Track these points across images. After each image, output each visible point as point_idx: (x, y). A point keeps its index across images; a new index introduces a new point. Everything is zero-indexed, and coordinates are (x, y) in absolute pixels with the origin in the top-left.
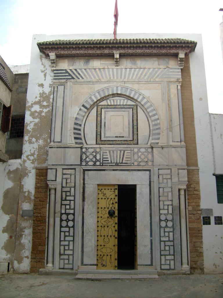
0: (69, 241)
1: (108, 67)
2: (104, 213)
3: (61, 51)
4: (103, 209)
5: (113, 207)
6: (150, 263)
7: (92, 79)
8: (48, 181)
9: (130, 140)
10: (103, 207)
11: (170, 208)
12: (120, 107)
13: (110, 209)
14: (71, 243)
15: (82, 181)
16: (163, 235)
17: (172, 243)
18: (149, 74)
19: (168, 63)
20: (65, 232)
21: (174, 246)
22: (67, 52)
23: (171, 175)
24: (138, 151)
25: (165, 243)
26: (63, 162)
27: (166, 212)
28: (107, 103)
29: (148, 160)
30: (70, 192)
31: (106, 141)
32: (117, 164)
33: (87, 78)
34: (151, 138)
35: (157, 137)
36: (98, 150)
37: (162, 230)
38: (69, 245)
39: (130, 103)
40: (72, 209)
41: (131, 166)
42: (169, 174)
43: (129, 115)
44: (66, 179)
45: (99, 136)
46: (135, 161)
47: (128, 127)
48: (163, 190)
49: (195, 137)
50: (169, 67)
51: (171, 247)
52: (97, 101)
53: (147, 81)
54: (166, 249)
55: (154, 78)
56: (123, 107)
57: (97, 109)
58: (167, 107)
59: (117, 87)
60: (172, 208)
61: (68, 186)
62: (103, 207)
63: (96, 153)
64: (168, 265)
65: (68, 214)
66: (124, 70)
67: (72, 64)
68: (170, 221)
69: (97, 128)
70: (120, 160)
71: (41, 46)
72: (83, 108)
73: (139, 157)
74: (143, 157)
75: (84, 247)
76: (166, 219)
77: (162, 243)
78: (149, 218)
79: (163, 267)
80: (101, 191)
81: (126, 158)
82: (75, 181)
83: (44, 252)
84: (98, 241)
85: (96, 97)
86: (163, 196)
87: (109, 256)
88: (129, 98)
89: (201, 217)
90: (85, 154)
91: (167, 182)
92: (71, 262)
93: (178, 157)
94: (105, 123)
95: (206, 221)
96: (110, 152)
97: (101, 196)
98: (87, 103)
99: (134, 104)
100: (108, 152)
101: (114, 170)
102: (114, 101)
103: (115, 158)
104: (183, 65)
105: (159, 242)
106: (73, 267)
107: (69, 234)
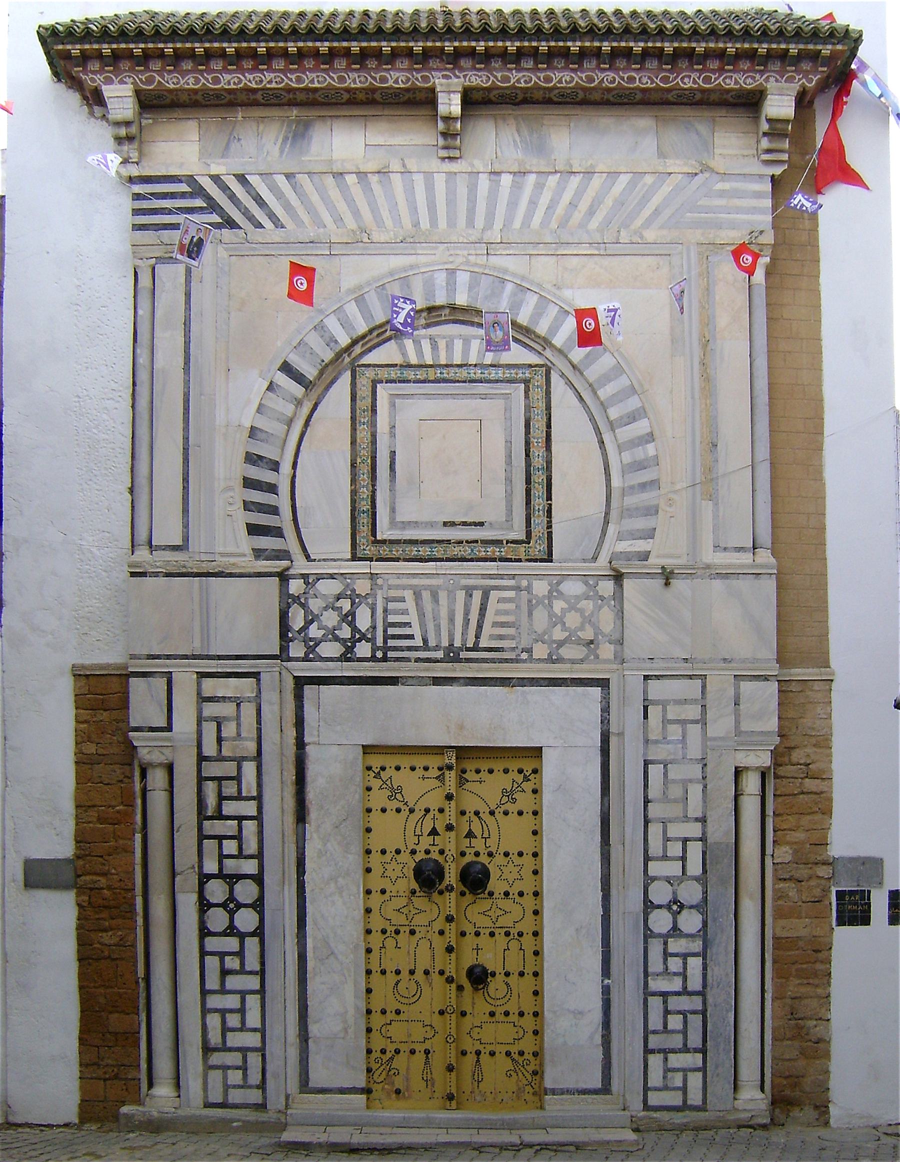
1: (404, 166)
3: (160, 73)
5: (437, 849)
11: (695, 851)
12: (463, 373)
13: (420, 856)
14: (253, 1001)
15: (291, 733)
17: (696, 1003)
18: (609, 202)
19: (708, 147)
20: (222, 955)
21: (704, 1013)
22: (192, 80)
25: (665, 1002)
26: (197, 644)
27: (673, 869)
28: (404, 354)
29: (596, 634)
31: (398, 542)
32: (452, 655)
33: (299, 223)
34: (612, 529)
35: (640, 524)
36: (362, 587)
37: (656, 948)
38: (242, 1011)
39: (517, 354)
40: (251, 857)
41: (517, 661)
42: (694, 701)
43: (508, 419)
44: (220, 723)
45: (364, 519)
48: (665, 774)
49: (822, 529)
50: (712, 170)
52: (354, 342)
54: (670, 1027)
55: (638, 222)
59: (452, 272)
60: (704, 853)
61: (225, 752)
63: (355, 598)
64: (678, 1089)
65: (232, 879)
66: (484, 182)
67: (226, 141)
68: (691, 907)
70: (464, 633)
71: (60, 47)
72: (282, 379)
73: (557, 620)
77: (655, 1003)
79: (654, 1099)
80: (377, 776)
81: (495, 624)
82: (259, 730)
84: (369, 991)
85: (346, 324)
86: (665, 798)
87: (420, 1057)
90: (303, 606)
91: (684, 736)
93: (740, 620)
94: (393, 454)
95: (850, 911)
96: (418, 596)
97: (379, 798)
99: (534, 359)
100: (408, 595)
101: (437, 681)
102: (434, 346)
103: (444, 624)
104: (785, 157)
106: (265, 1098)
107: (242, 964)
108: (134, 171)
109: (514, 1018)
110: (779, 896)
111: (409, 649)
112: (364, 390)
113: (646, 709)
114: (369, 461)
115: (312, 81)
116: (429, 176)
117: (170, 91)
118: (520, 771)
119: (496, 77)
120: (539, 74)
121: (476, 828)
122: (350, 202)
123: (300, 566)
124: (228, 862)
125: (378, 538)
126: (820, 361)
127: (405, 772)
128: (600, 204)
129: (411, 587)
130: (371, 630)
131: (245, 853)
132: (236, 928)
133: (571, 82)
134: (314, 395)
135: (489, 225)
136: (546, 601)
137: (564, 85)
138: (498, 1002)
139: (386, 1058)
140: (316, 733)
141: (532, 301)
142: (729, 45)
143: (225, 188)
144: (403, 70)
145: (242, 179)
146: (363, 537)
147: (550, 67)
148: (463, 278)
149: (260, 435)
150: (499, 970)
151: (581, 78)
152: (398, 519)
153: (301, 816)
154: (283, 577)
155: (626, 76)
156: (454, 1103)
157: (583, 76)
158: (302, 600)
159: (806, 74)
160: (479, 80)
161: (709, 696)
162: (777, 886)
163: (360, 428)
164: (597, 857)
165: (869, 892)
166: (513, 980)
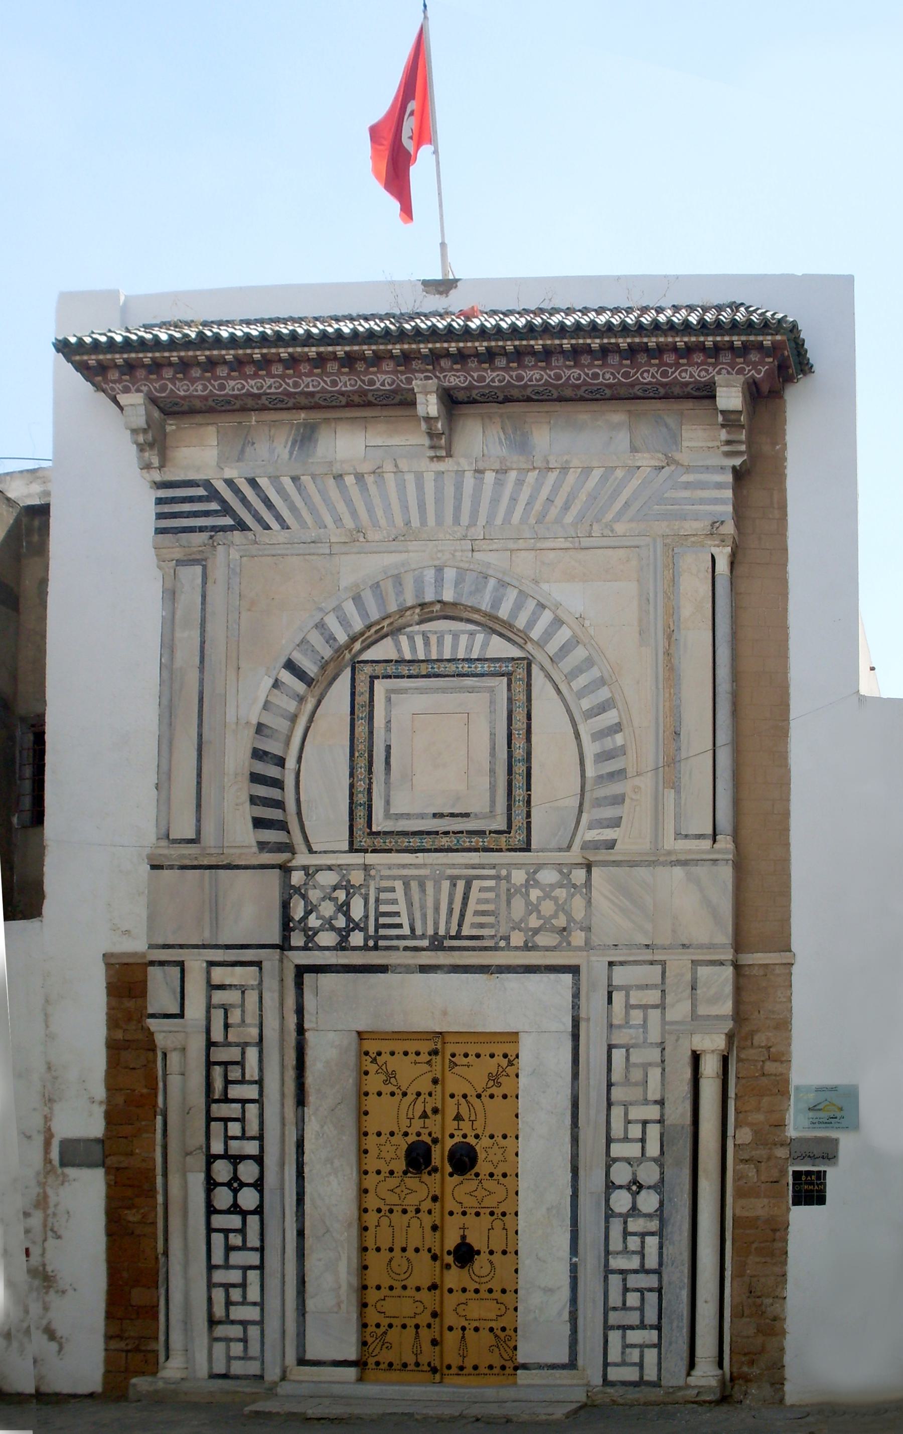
0: (245, 1269)
1: (396, 466)
2: (499, 1157)
3: (173, 380)
4: (383, 1139)
6: (565, 1359)
7: (326, 527)
8: (153, 1016)
9: (496, 832)
10: (385, 1131)
11: (653, 1131)
12: (451, 668)
13: (412, 1138)
14: (253, 1276)
15: (292, 1020)
16: (620, 1247)
17: (652, 1281)
18: (583, 496)
19: (675, 439)
20: (226, 1232)
21: (660, 1290)
22: (200, 387)
23: (663, 991)
24: (527, 881)
25: (624, 1280)
27: (633, 1150)
28: (399, 650)
29: (568, 922)
30: (241, 1064)
32: (437, 944)
33: (303, 524)
34: (585, 817)
35: (609, 812)
36: (357, 878)
37: (616, 1227)
38: (243, 1285)
39: (499, 648)
40: (253, 1138)
41: (496, 948)
42: (655, 986)
43: (493, 711)
44: (226, 1010)
45: (361, 812)
46: (514, 929)
47: (487, 767)
48: (627, 1058)
49: (787, 814)
50: (677, 463)
51: (648, 1295)
52: (353, 639)
53: (575, 534)
54: (628, 1304)
55: (609, 516)
56: (465, 668)
57: (353, 679)
58: (661, 670)
59: (439, 570)
60: (662, 1135)
61: (231, 1038)
62: (385, 1131)
63: (350, 889)
64: (634, 1364)
65: (236, 1160)
66: (469, 480)
67: (240, 448)
68: (649, 1187)
69: (352, 775)
70: (448, 922)
72: (286, 677)
73: (533, 908)
74: (547, 908)
75: (307, 1295)
76: (635, 1182)
77: (615, 1281)
78: (569, 1176)
79: (614, 1374)
80: (374, 1061)
81: (477, 913)
82: (261, 1016)
83: (152, 1312)
84: (516, 1271)
85: (344, 622)
86: (627, 1081)
87: (411, 1331)
88: (494, 625)
89: (787, 1172)
90: (304, 897)
92: (254, 1349)
93: (695, 904)
94: (388, 748)
95: (806, 1191)
96: (407, 885)
97: (374, 1082)
98: (305, 654)
99: (516, 653)
100: (399, 885)
101: (424, 969)
102: (427, 643)
103: (430, 913)
105: (602, 1274)
106: (263, 1369)
107: (244, 1241)
108: (158, 477)
109: (497, 1295)
110: (738, 1177)
111: (398, 937)
112: (362, 687)
113: (610, 994)
114: (366, 755)
115: (307, 386)
116: (419, 477)
117: (184, 398)
118: (505, 1056)
119: (472, 377)
120: (511, 373)
121: (464, 1111)
122: (349, 503)
123: (302, 858)
124: (233, 1144)
125: (374, 830)
126: (787, 649)
127: (399, 1056)
128: (574, 499)
129: (400, 877)
130: (363, 919)
131: (248, 1134)
132: (239, 1206)
133: (540, 380)
134: (317, 691)
135: (473, 524)
136: (524, 890)
137: (534, 383)
138: (483, 1280)
139: (380, 1331)
140: (314, 1020)
141: (511, 595)
142: (678, 339)
143: (237, 491)
144: (388, 372)
145: (253, 482)
146: (360, 829)
147: (521, 366)
148: (450, 574)
149: (266, 731)
150: (484, 1249)
151: (550, 376)
152: (392, 812)
153: (301, 1100)
154: (285, 869)
155: (590, 372)
156: (438, 1376)
157: (552, 373)
158: (303, 891)
159: (755, 365)
160: (457, 380)
161: (667, 981)
162: (738, 1167)
163: (358, 723)
164: (568, 1138)
165: (825, 1172)
166: (497, 1258)
